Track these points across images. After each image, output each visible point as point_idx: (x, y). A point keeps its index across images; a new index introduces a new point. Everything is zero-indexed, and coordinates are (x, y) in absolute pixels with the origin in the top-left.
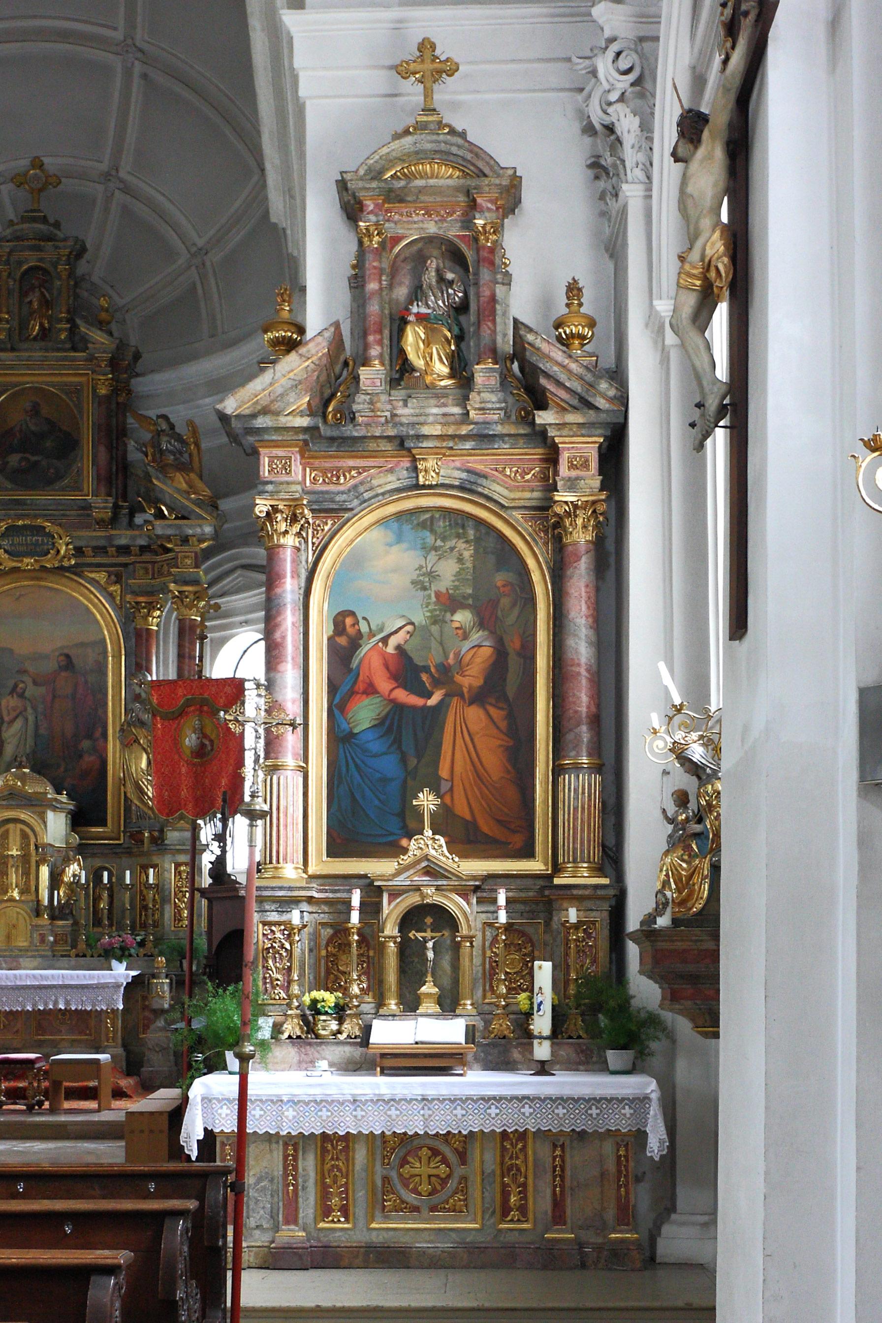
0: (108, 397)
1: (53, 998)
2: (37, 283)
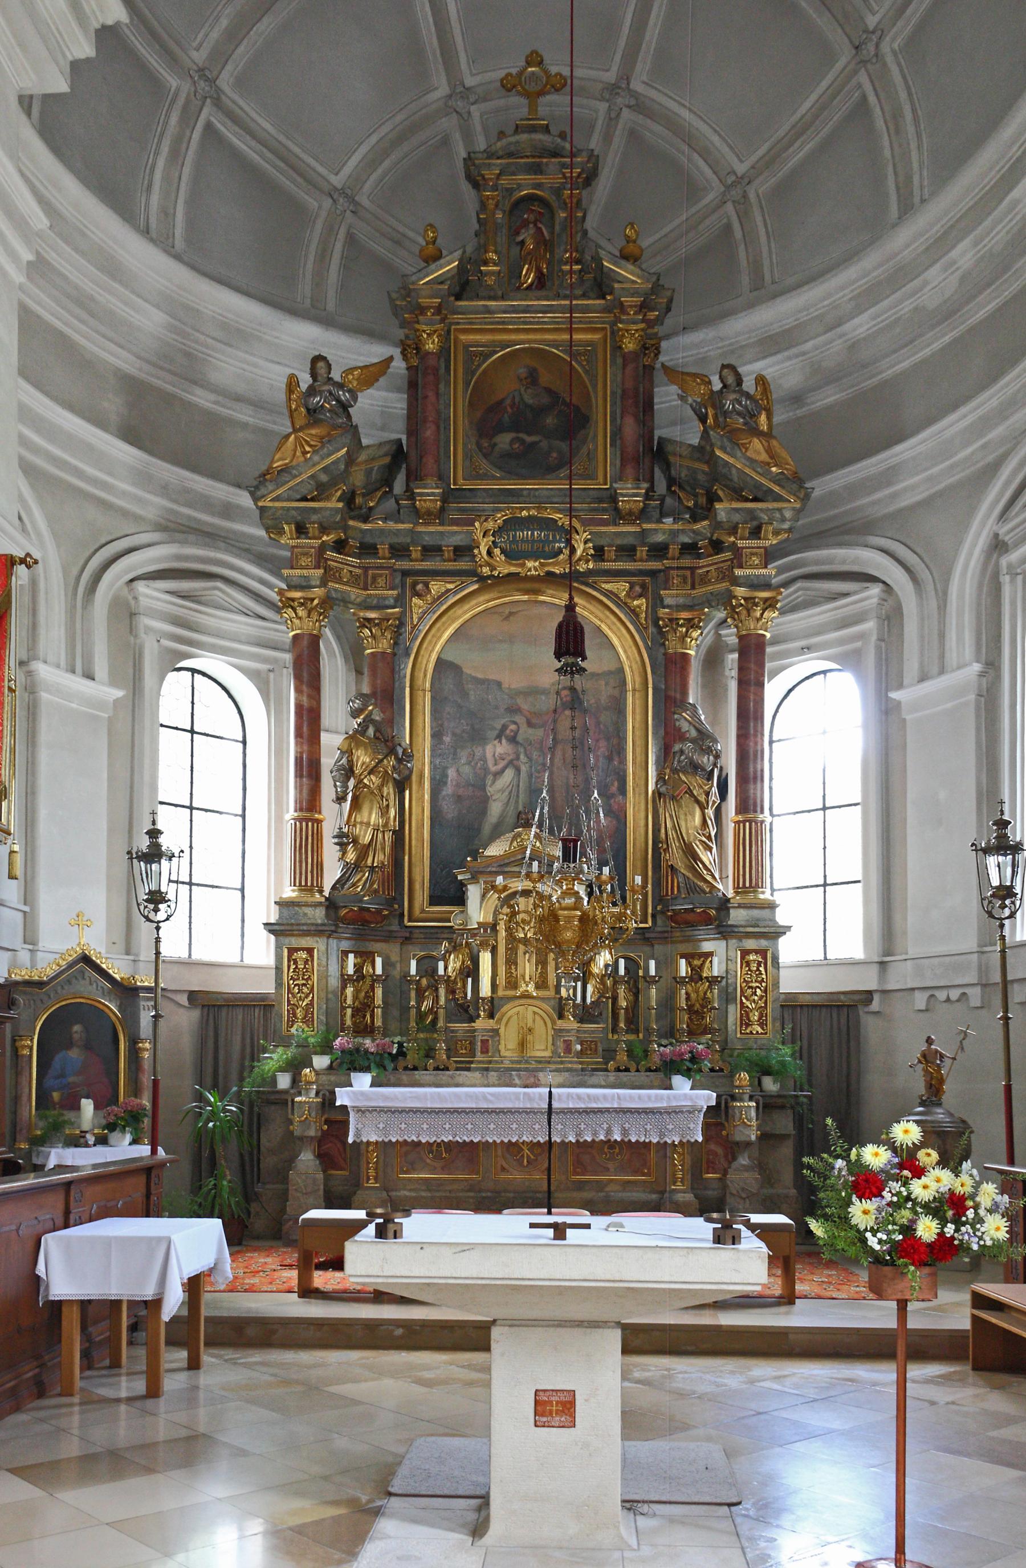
0: (635, 355)
1: (605, 1126)
2: (532, 217)
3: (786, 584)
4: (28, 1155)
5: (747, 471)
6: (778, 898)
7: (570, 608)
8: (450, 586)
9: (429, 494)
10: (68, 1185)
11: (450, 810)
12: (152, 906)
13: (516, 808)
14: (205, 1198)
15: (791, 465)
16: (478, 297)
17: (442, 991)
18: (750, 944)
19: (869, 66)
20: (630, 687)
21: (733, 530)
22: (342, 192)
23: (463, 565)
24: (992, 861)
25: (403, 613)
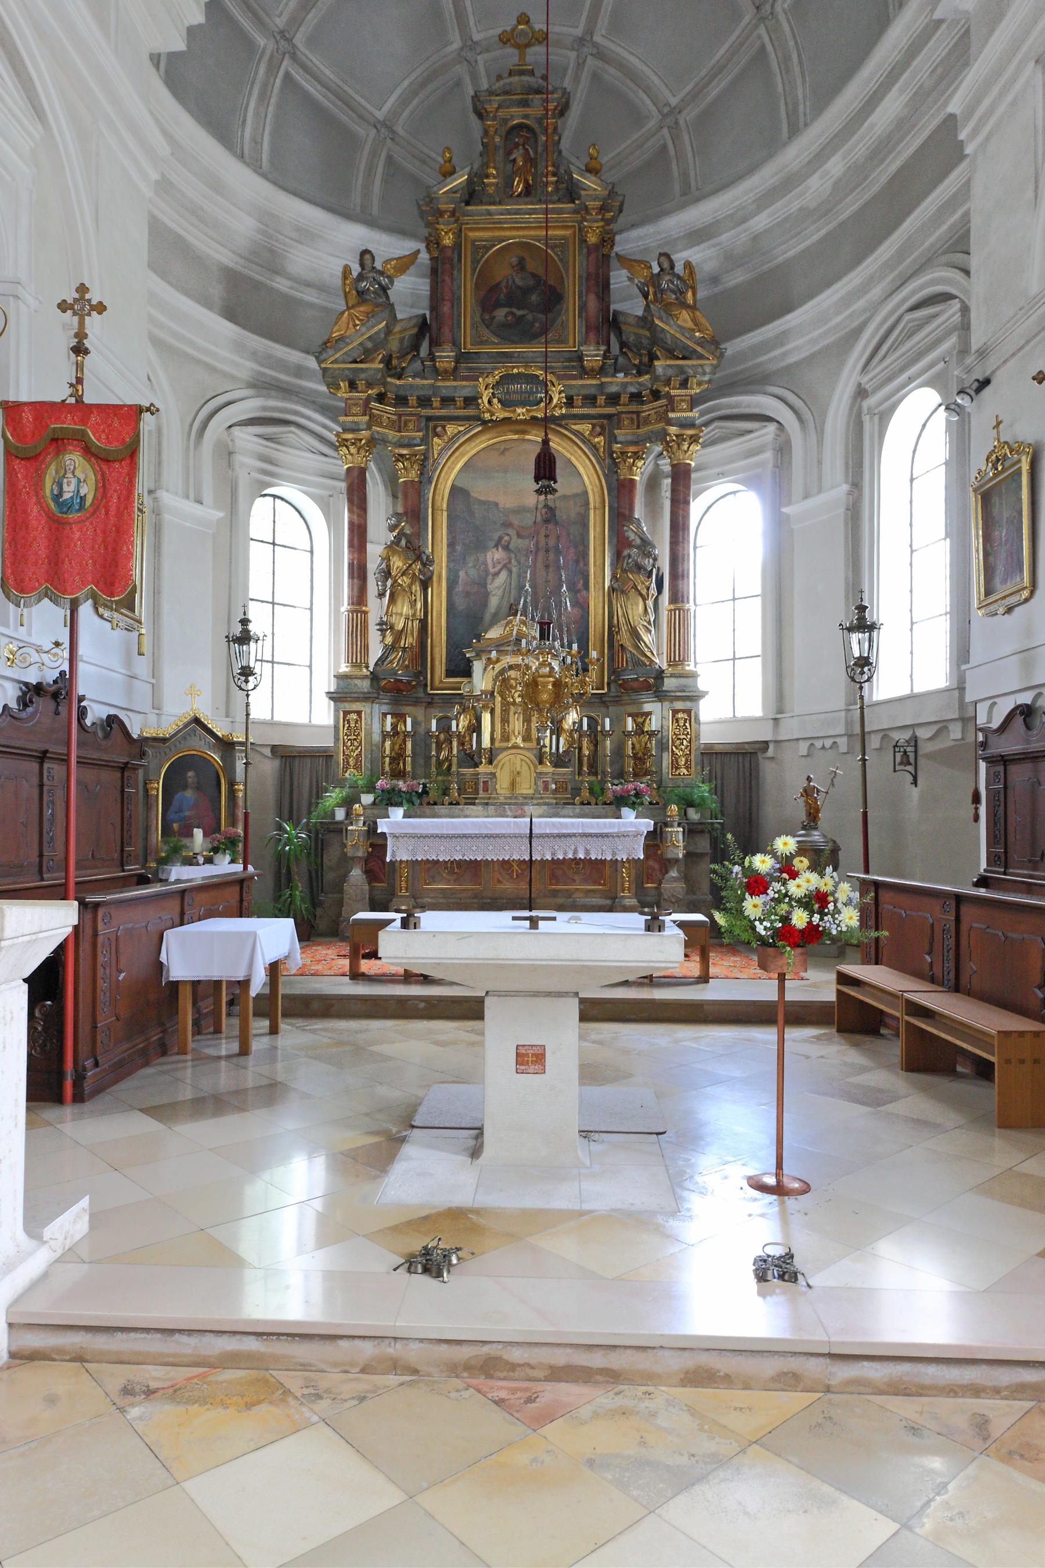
0: (596, 247)
1: (573, 847)
2: (521, 141)
3: (706, 424)
4: (156, 873)
5: (678, 335)
6: (699, 670)
7: (546, 442)
8: (461, 428)
9: (446, 357)
10: (183, 892)
11: (461, 604)
12: (243, 678)
13: (509, 601)
14: (284, 905)
15: (710, 331)
16: (482, 203)
17: (455, 744)
18: (679, 705)
19: (767, 21)
20: (592, 506)
21: (668, 382)
22: (383, 124)
23: (470, 412)
24: (855, 637)
25: (427, 450)
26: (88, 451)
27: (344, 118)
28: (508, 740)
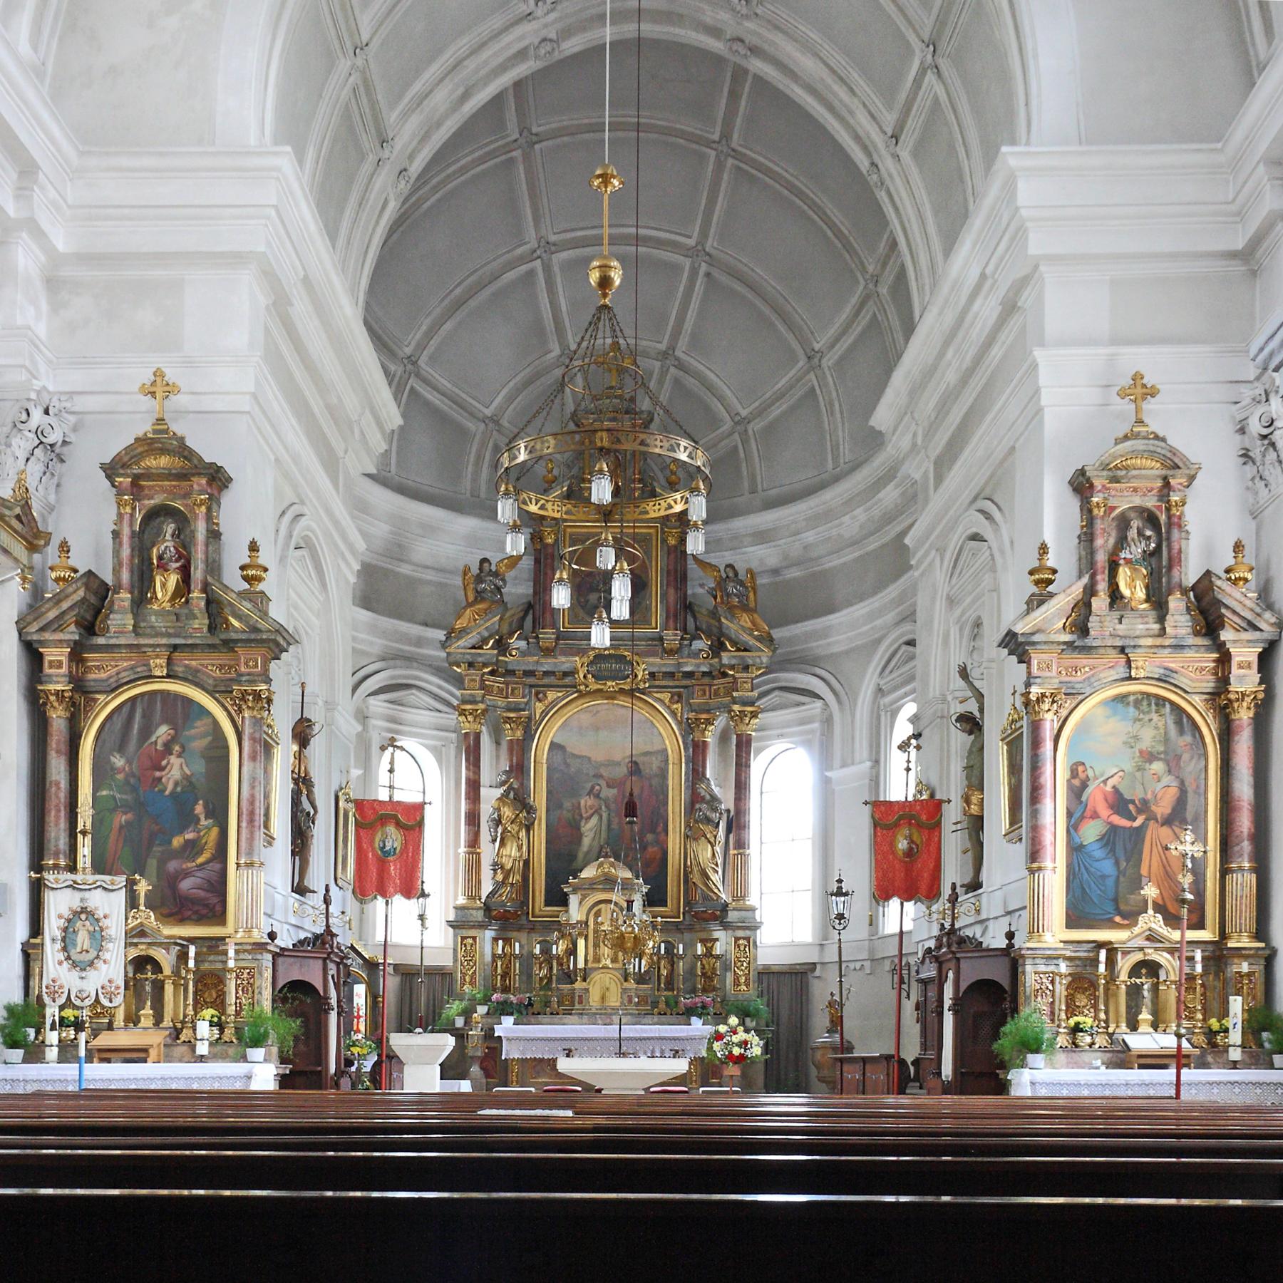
18: (740, 933)
20: (670, 762)
26: (398, 824)
27: (459, 418)
28: (599, 961)
